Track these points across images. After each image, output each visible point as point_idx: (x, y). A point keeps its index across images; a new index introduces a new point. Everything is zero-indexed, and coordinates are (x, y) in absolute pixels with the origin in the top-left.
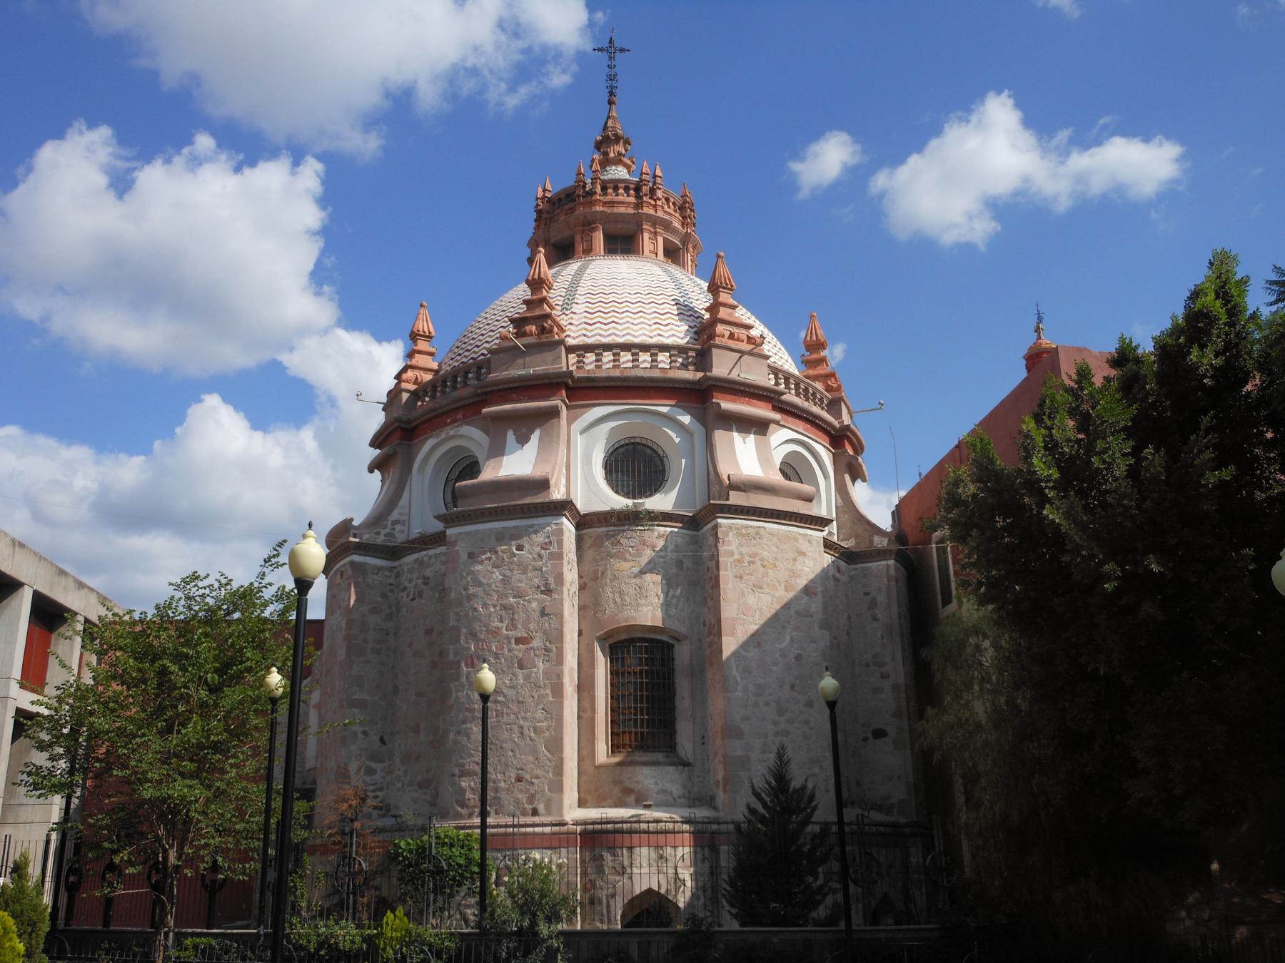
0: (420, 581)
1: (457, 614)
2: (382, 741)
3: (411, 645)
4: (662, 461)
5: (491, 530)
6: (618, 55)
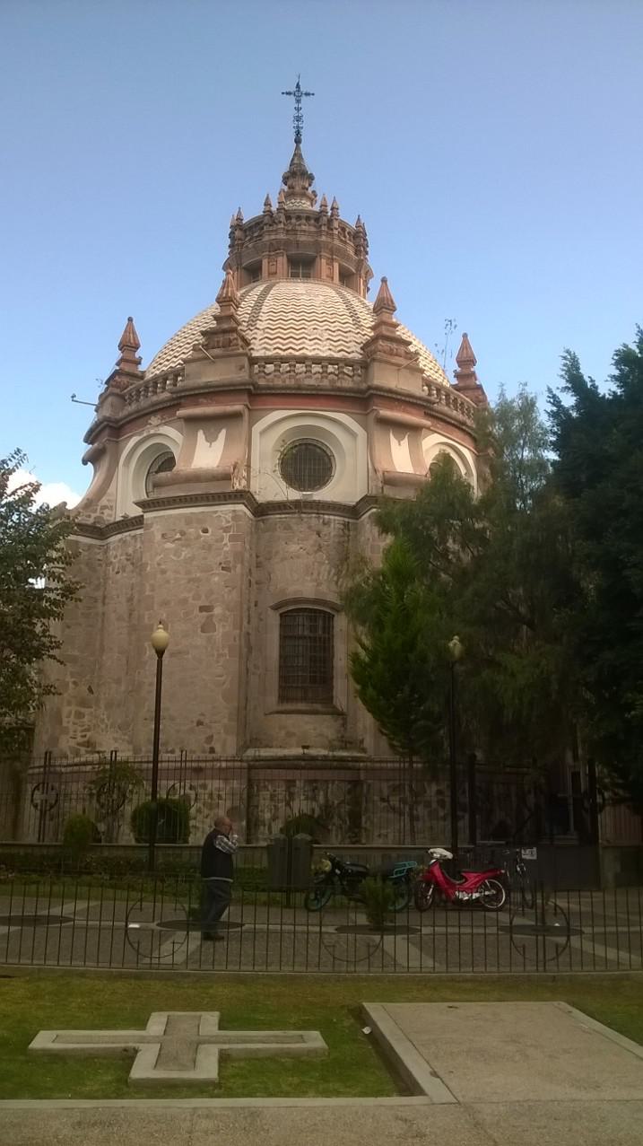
1: (152, 586)
2: (90, 690)
4: (330, 460)
6: (304, 98)
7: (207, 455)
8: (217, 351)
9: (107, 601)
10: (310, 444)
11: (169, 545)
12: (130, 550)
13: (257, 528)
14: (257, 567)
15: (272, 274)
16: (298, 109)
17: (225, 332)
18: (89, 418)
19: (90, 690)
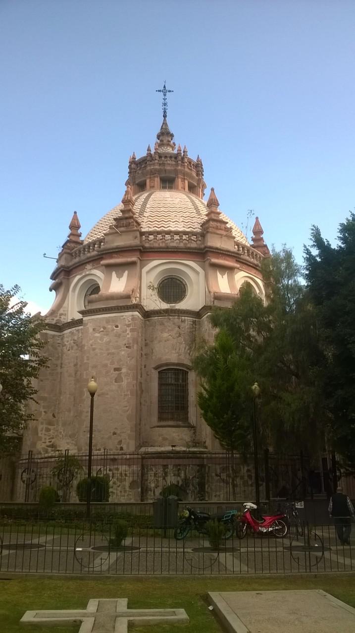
0: (72, 342)
1: (88, 357)
2: (54, 416)
3: (67, 372)
5: (104, 318)
7: (117, 285)
8: (122, 229)
9: (63, 366)
10: (174, 278)
11: (97, 335)
12: (76, 338)
13: (145, 324)
14: (145, 346)
15: (152, 187)
16: (165, 99)
17: (127, 218)
18: (53, 266)
19: (54, 416)
